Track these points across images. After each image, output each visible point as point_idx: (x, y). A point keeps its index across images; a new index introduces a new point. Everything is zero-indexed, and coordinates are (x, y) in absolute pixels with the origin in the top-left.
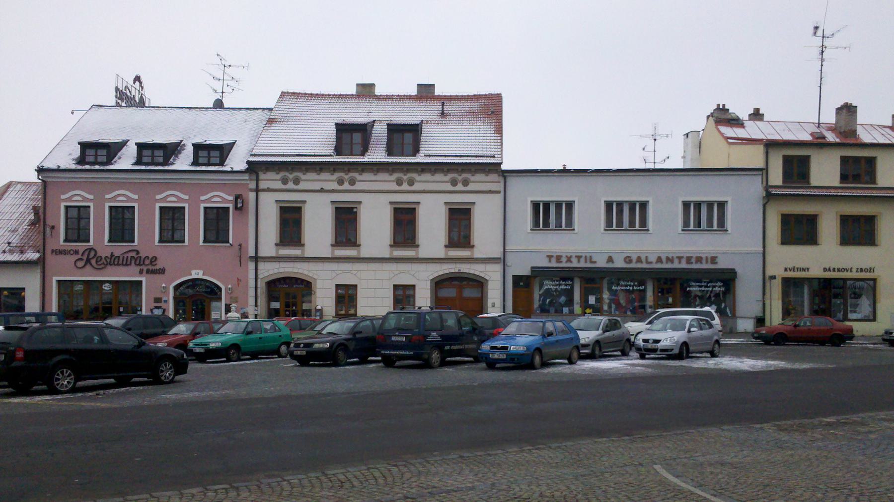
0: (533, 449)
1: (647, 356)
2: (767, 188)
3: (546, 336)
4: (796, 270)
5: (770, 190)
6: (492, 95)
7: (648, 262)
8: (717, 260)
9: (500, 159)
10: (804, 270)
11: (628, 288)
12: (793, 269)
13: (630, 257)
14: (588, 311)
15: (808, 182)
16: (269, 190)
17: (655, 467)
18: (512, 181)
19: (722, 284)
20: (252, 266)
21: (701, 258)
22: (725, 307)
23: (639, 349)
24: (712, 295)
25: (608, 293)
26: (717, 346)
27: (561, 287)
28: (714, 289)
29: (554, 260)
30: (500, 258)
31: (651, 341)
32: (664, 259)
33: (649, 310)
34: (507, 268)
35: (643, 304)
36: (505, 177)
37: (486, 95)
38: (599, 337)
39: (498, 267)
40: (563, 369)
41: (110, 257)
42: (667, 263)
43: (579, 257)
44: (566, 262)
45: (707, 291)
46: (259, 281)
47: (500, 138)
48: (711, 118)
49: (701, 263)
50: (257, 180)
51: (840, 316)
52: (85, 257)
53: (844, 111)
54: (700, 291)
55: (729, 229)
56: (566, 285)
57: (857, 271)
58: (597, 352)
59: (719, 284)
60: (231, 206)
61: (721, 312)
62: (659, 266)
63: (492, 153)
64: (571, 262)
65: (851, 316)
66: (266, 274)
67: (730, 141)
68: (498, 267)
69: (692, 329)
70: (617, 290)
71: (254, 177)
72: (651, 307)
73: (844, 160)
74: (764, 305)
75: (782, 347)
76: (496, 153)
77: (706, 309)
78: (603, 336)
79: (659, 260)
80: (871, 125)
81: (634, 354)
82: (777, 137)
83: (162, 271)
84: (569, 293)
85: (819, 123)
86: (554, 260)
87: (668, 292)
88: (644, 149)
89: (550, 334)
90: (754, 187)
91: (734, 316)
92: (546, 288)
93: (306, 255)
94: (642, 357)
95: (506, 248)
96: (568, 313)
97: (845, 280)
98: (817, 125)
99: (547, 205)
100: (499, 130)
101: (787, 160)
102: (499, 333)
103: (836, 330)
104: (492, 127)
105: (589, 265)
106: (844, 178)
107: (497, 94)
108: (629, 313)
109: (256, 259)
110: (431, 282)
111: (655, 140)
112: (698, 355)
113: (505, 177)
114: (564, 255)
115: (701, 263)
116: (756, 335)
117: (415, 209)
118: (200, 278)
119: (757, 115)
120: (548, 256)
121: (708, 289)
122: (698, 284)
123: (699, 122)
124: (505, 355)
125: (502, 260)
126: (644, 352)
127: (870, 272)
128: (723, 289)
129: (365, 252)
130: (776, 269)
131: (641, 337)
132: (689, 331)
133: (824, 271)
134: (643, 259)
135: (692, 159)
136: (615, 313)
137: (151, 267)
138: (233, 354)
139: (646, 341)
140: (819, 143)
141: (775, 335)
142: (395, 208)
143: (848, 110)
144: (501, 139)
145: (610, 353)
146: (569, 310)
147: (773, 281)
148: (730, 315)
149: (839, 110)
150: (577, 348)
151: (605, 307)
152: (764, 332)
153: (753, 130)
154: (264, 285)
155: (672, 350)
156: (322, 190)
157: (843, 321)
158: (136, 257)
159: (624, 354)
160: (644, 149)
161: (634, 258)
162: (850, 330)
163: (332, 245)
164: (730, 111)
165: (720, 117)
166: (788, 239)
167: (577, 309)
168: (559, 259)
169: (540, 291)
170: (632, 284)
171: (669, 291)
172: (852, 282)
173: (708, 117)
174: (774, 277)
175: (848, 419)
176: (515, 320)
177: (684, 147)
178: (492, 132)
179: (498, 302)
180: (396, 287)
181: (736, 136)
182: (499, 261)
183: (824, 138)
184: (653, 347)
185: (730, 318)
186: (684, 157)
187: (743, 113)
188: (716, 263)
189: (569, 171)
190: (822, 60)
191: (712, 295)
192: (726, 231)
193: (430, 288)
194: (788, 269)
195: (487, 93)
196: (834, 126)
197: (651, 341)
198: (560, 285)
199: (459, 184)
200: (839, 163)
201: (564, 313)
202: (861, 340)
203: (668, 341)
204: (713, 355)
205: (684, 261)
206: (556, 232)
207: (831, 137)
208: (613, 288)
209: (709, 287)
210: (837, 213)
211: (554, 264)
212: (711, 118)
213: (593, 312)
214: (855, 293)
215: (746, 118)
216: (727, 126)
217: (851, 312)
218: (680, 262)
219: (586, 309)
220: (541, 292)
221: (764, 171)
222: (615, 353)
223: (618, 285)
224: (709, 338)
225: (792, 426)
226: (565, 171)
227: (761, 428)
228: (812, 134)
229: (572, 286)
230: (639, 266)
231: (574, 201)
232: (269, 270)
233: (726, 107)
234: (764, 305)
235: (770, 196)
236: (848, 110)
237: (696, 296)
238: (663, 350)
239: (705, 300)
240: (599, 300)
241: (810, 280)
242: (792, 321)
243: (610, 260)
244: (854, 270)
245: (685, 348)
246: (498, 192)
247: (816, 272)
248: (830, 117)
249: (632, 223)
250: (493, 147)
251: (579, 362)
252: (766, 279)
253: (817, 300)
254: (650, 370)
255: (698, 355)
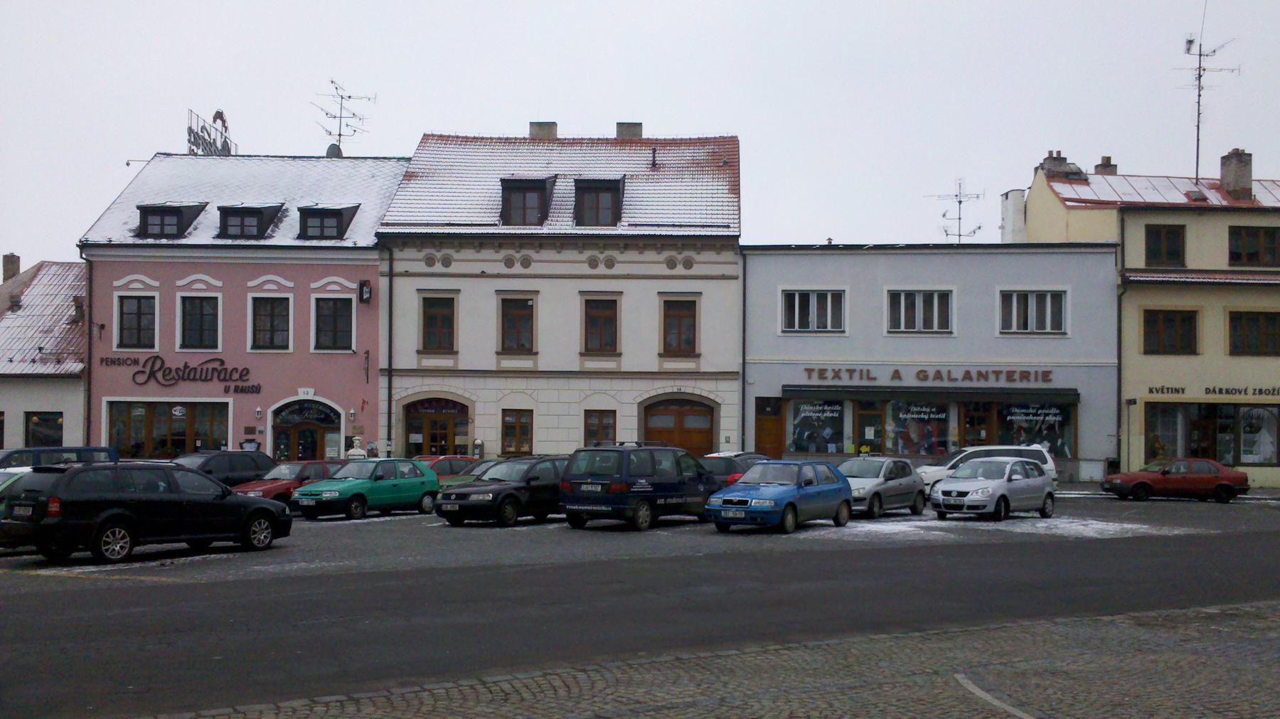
0: (781, 649)
1: (948, 516)
2: (1124, 272)
3: (803, 485)
4: (1165, 390)
5: (1128, 275)
6: (724, 138)
7: (950, 379)
8: (1052, 376)
9: (737, 230)
10: (1177, 391)
11: (922, 416)
12: (1162, 390)
13: (926, 371)
14: (864, 449)
15: (1183, 265)
16: (407, 274)
17: (957, 676)
18: (755, 262)
19: (1058, 411)
20: (383, 382)
21: (1028, 373)
22: (1063, 444)
23: (936, 506)
24: (1044, 427)
25: (892, 422)
26: (1049, 501)
27: (825, 415)
28: (1047, 418)
29: (815, 375)
30: (738, 372)
31: (954, 494)
32: (974, 375)
33: (952, 449)
34: (747, 387)
35: (943, 439)
36: (744, 257)
37: (715, 138)
38: (878, 488)
39: (735, 386)
40: (827, 534)
41: (182, 369)
42: (978, 380)
43: (851, 372)
44: (833, 378)
45: (1037, 421)
46: (394, 404)
47: (736, 200)
48: (1040, 171)
49: (1029, 380)
50: (391, 260)
51: (1229, 458)
52: (148, 370)
53: (1234, 161)
54: (1026, 421)
55: (1069, 331)
56: (832, 411)
57: (1254, 394)
58: (876, 509)
59: (1054, 411)
60: (354, 297)
61: (1056, 452)
62: (967, 384)
63: (725, 221)
64: (840, 378)
65: (1245, 458)
66: (404, 394)
67: (1068, 203)
68: (735, 386)
69: (1014, 477)
70: (906, 419)
71: (386, 256)
72: (954, 444)
73: (1235, 232)
74: (1119, 442)
75: (1145, 503)
76: (732, 221)
77: (1035, 447)
78: (883, 486)
79: (967, 376)
80: (1272, 181)
81: (929, 512)
82: (1137, 199)
83: (256, 390)
84: (838, 423)
85: (1197, 179)
86: (815, 375)
87: (979, 424)
88: (944, 215)
89: (809, 483)
90: (1105, 271)
91: (1075, 457)
92: (803, 415)
93: (623, 369)
94: (942, 517)
95: (747, 358)
96: (834, 452)
97: (1236, 406)
98: (1194, 181)
99: (805, 296)
100: (735, 189)
101: (1152, 232)
102: (736, 481)
103: (1223, 479)
104: (724, 183)
105: (865, 383)
106: (1235, 257)
107: (732, 137)
108: (923, 453)
109: (390, 372)
110: (638, 406)
111: (960, 202)
112: (1022, 514)
113: (744, 257)
114: (830, 368)
115: (1029, 380)
116: (1107, 486)
117: (453, 299)
118: (310, 399)
119: (1107, 167)
120: (806, 370)
121: (1038, 418)
122: (1024, 411)
123: (1024, 178)
124: (743, 513)
125: (741, 376)
126: (944, 510)
127: (1273, 394)
128: (1059, 418)
129: (544, 363)
130: (1137, 389)
131: (940, 487)
132: (1010, 480)
133: (1206, 393)
134: (945, 375)
135: (1013, 230)
136: (903, 452)
137: (240, 384)
138: (356, 507)
139: (947, 493)
140: (1197, 207)
141: (1134, 486)
142: (425, 299)
143: (1238, 160)
144: (739, 201)
145: (894, 511)
146: (837, 447)
147: (1132, 407)
148: (1069, 456)
149: (1225, 160)
150: (847, 502)
151: (889, 444)
152: (1118, 481)
153: (1101, 188)
154: (401, 410)
155: (984, 507)
156: (483, 275)
157: (1233, 466)
158: (219, 368)
159: (916, 512)
160: (944, 215)
161: (931, 374)
162: (1244, 479)
163: (498, 353)
164: (1068, 161)
165: (1053, 169)
166: (1153, 346)
167: (849, 446)
168: (822, 374)
169: (795, 419)
170: (928, 410)
171: (982, 421)
172: (1246, 409)
173: (1036, 169)
174: (1132, 402)
175: (1237, 609)
176: (757, 462)
177: (1003, 213)
178: (725, 191)
179: (735, 436)
180: (588, 413)
181: (1078, 197)
182: (736, 377)
183: (1205, 199)
184: (958, 503)
185: (1070, 460)
186: (1002, 227)
187: (1087, 164)
188: (1050, 380)
189: (836, 247)
190: (1200, 88)
191: (1044, 427)
192: (1065, 334)
193: (636, 415)
194: (1154, 390)
195: (717, 136)
196: (1218, 182)
197: (954, 494)
198: (824, 411)
199: (516, 264)
200: (1226, 235)
201: (829, 452)
202: (1258, 494)
203: (980, 494)
204: (1044, 514)
205: (1003, 377)
206: (819, 335)
207: (1215, 199)
208: (901, 416)
209: (1039, 415)
210: (1225, 308)
211: (815, 381)
212: (1040, 171)
213: (871, 451)
214: (1251, 426)
215: (1092, 171)
216: (1064, 183)
217: (1246, 452)
218: (997, 379)
219: (861, 445)
220: (796, 422)
221: (1119, 249)
222: (903, 511)
223: (908, 411)
224: (1041, 488)
225: (1156, 618)
226: (830, 248)
227: (1112, 622)
228: (1187, 195)
229: (841, 413)
230: (938, 384)
231: (844, 291)
232: (408, 388)
233: (1063, 155)
234: (1119, 442)
235: (1127, 284)
236: (1238, 160)
237: (1020, 428)
238: (970, 507)
239: (1034, 435)
240: (880, 433)
241: (1185, 406)
242: (1160, 465)
243: (896, 375)
244: (1250, 391)
245: (1003, 504)
246: (736, 278)
247: (1195, 394)
248: (1212, 170)
249: (928, 322)
250: (727, 212)
251: (849, 524)
252: (1123, 405)
253: (1196, 435)
254: (952, 536)
255: (1022, 514)
